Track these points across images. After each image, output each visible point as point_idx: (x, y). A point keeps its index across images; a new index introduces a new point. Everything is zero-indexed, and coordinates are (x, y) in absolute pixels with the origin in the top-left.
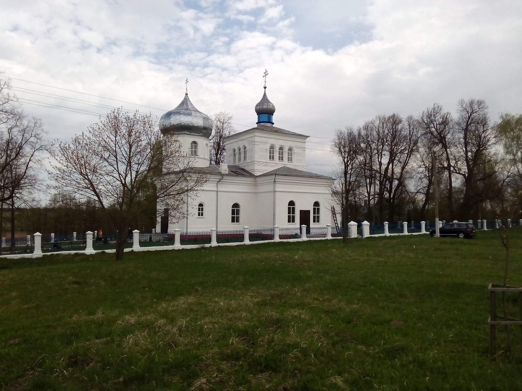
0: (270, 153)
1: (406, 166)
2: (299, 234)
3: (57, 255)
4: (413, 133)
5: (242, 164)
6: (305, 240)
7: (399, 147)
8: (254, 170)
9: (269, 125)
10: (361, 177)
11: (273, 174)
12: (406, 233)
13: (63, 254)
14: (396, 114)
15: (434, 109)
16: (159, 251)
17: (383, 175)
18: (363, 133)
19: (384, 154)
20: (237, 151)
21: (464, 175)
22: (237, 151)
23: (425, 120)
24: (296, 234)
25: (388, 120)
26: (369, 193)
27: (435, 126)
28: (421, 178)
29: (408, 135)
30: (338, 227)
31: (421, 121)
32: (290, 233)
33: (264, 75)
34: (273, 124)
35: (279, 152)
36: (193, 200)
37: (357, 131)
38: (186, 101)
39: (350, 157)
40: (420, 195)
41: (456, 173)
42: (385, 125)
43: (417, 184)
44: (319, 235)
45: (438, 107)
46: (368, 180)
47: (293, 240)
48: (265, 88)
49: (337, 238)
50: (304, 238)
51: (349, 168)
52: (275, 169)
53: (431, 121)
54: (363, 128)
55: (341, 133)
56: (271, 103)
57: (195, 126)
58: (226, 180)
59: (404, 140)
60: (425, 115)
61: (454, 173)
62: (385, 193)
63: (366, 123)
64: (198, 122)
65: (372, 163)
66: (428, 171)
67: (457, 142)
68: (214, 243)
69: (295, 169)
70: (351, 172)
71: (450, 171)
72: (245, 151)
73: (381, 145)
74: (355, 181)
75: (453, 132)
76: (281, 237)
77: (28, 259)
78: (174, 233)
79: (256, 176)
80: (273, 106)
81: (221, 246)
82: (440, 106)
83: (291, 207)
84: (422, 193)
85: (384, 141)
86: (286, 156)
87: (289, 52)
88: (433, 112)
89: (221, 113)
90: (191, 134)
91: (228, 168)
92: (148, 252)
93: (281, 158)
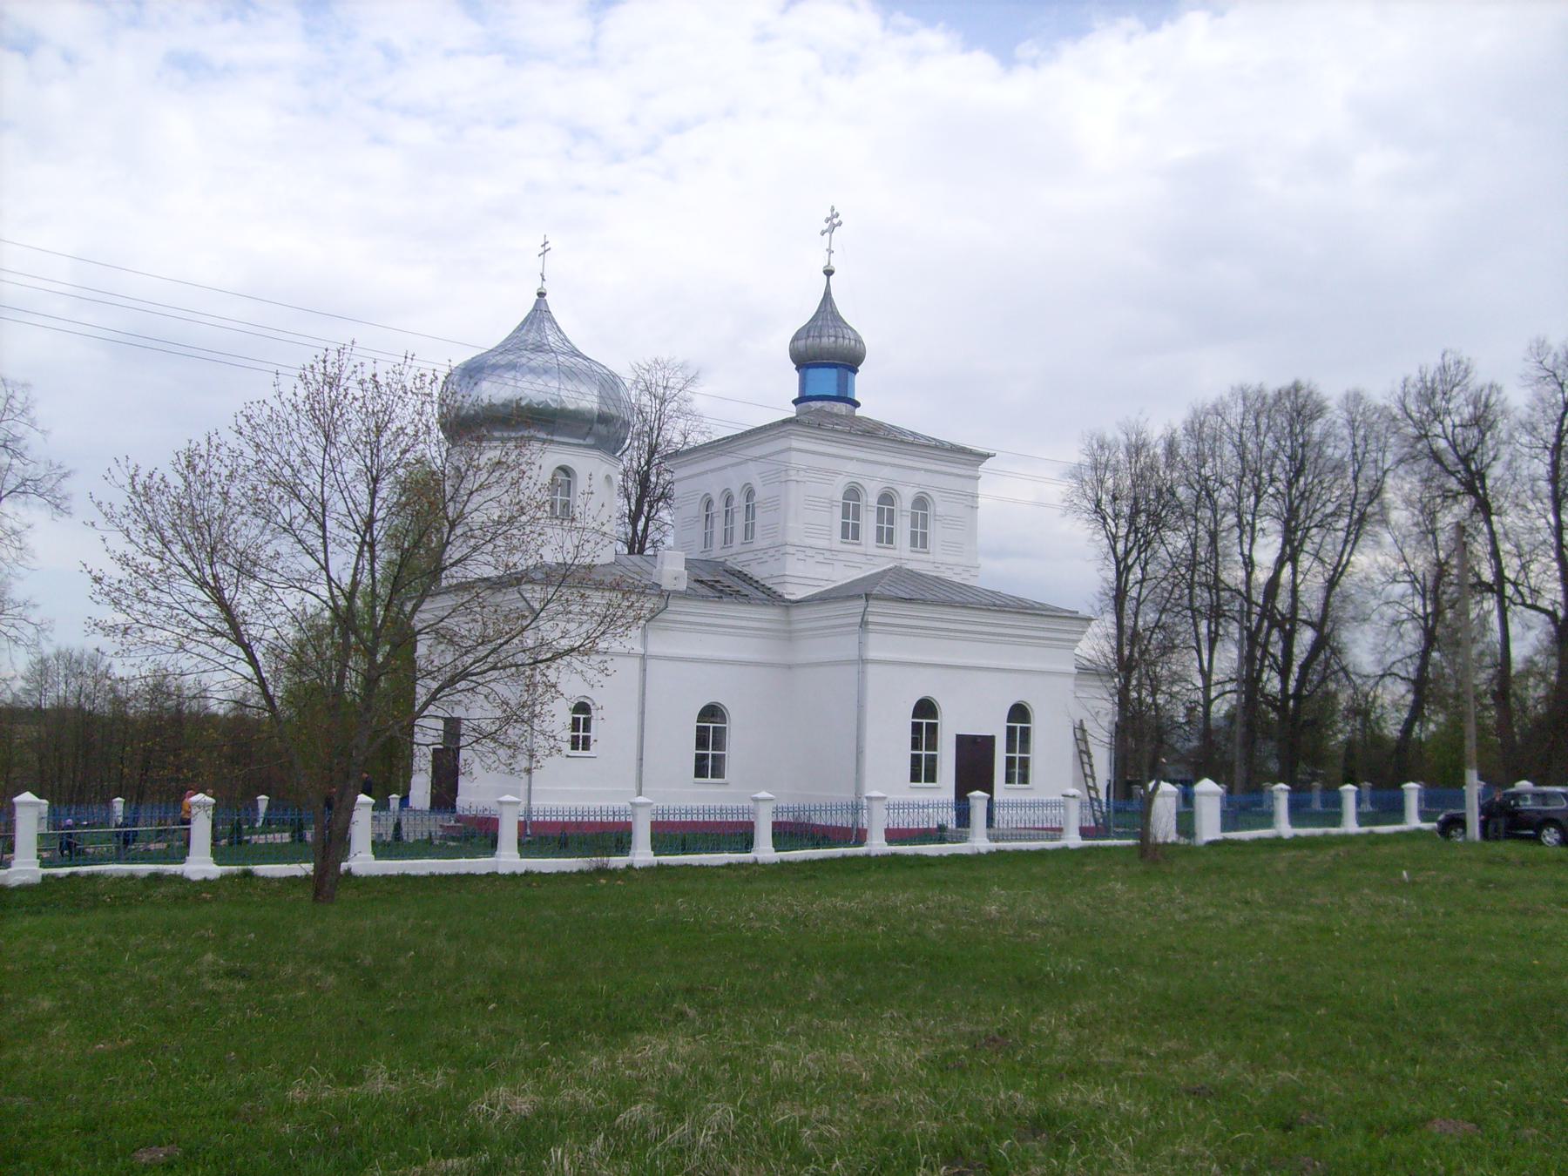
0: (845, 515)
1: (1341, 574)
2: (950, 826)
3: (92, 877)
4: (1364, 454)
5: (737, 556)
6: (983, 851)
7: (1318, 506)
9: (841, 408)
10: (1179, 612)
11: (859, 597)
12: (1350, 826)
13: (111, 876)
14: (1304, 381)
15: (1444, 369)
16: (441, 875)
17: (1257, 605)
18: (1185, 448)
19: (1262, 530)
20: (718, 506)
21: (1552, 615)
22: (718, 506)
23: (1412, 407)
24: (942, 828)
25: (1275, 403)
26: (1206, 675)
27: (1449, 430)
28: (1396, 623)
29: (1346, 459)
30: (1100, 802)
31: (1396, 411)
32: (916, 820)
33: (826, 226)
34: (857, 404)
35: (880, 512)
36: (589, 688)
37: (1163, 441)
39: (1136, 536)
40: (1393, 683)
41: (1524, 604)
42: (1263, 420)
43: (1384, 645)
44: (1027, 831)
45: (1459, 363)
46: (1203, 628)
47: (273, 869)
48: (829, 273)
49: (1101, 842)
50: (979, 842)
51: (1131, 577)
52: (861, 576)
53: (1434, 411)
54: (1186, 429)
55: (1101, 447)
57: (570, 411)
58: (680, 613)
59: (1336, 480)
60: (1413, 391)
61: (1515, 604)
62: (1265, 677)
63: (1195, 412)
64: (585, 399)
65: (1217, 561)
66: (1424, 597)
67: (1524, 491)
68: (642, 854)
69: (937, 577)
70: (1140, 594)
71: (1502, 597)
72: (748, 506)
73: (1248, 497)
74: (1154, 628)
75: (1512, 455)
76: (893, 836)
77: (855, 858)
78: (495, 807)
79: (790, 601)
80: (858, 340)
81: (668, 865)
82: (1465, 360)
83: (924, 721)
84: (1402, 679)
85: (1260, 478)
86: (903, 528)
88: (1441, 380)
89: (656, 362)
90: (556, 438)
91: (686, 568)
92: (404, 878)
93: (885, 536)
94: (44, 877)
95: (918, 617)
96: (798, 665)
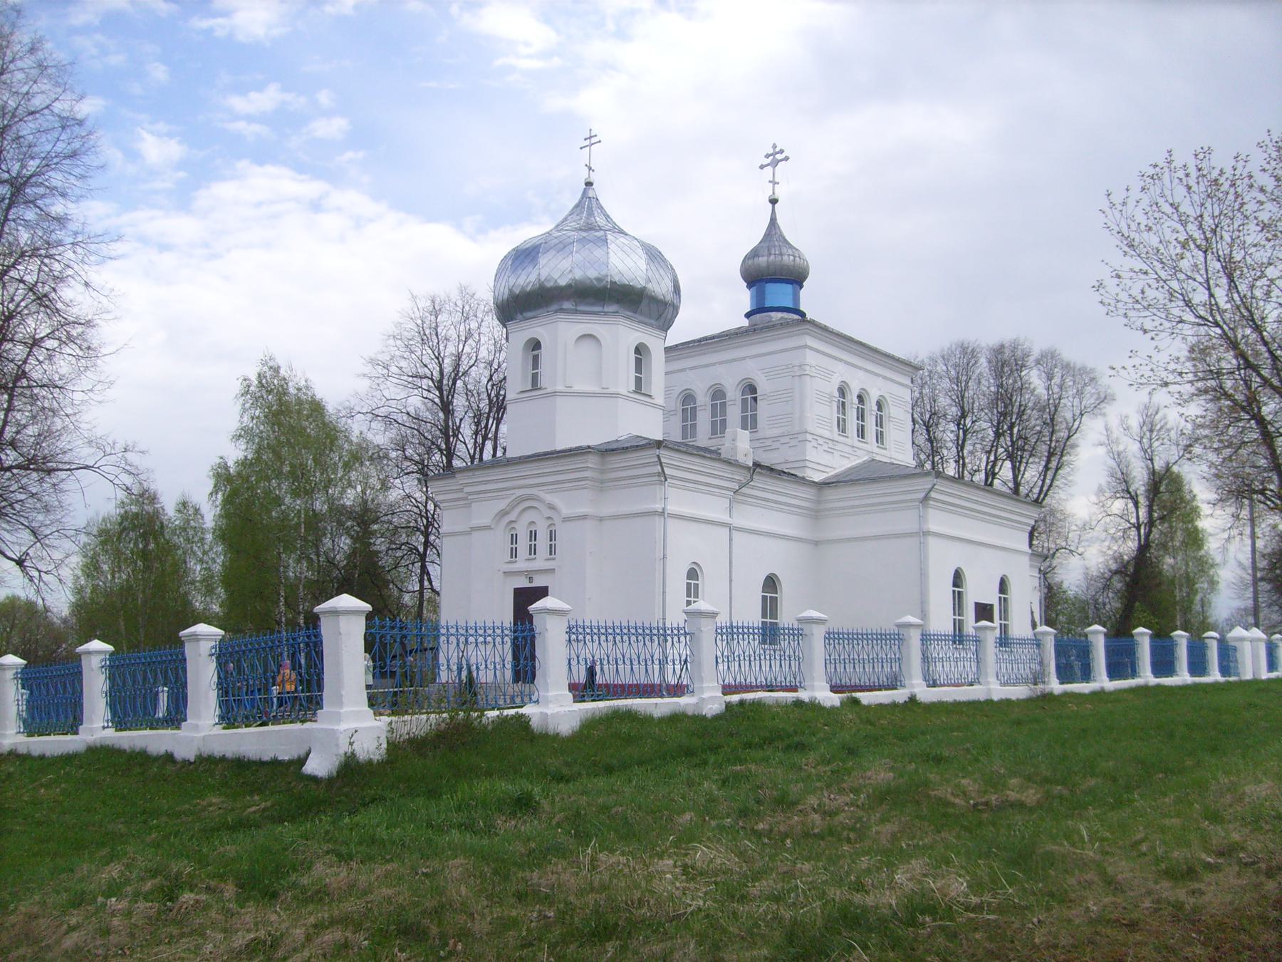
8: (803, 463)
38: (588, 202)
48: (774, 201)
56: (797, 250)
58: (763, 490)
87: (359, 223)
94: (729, 706)
95: (961, 497)
96: (828, 541)
